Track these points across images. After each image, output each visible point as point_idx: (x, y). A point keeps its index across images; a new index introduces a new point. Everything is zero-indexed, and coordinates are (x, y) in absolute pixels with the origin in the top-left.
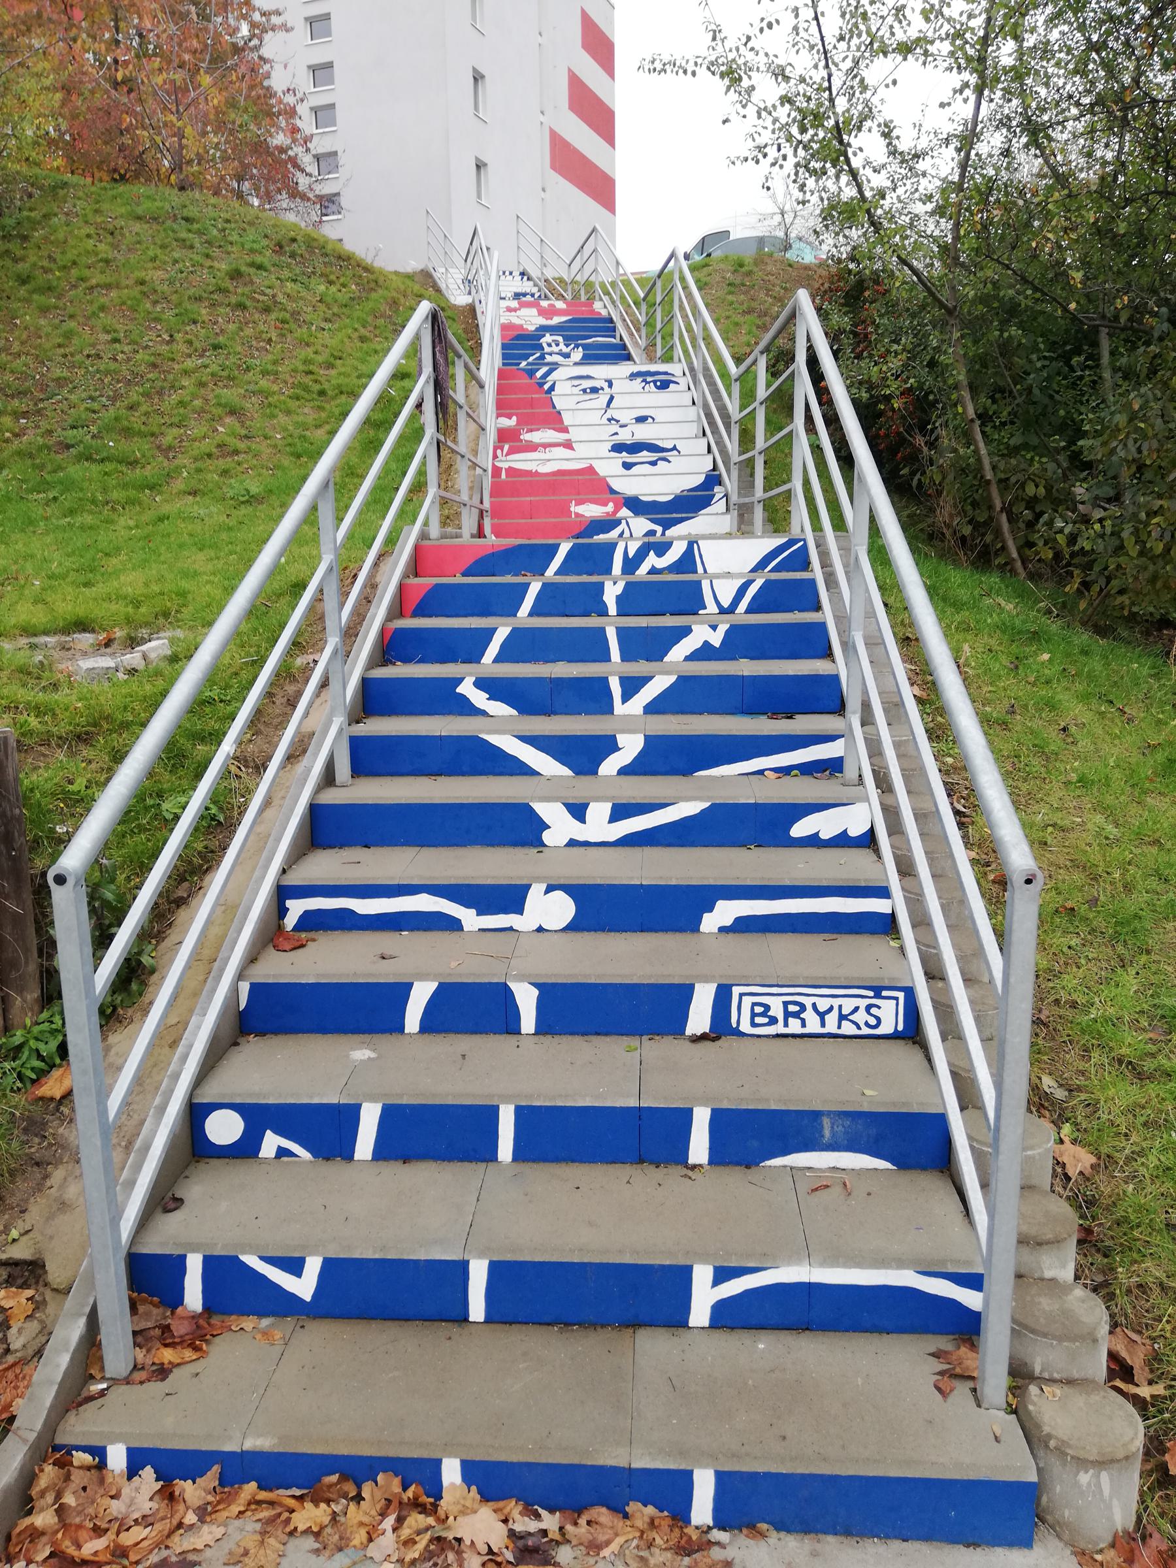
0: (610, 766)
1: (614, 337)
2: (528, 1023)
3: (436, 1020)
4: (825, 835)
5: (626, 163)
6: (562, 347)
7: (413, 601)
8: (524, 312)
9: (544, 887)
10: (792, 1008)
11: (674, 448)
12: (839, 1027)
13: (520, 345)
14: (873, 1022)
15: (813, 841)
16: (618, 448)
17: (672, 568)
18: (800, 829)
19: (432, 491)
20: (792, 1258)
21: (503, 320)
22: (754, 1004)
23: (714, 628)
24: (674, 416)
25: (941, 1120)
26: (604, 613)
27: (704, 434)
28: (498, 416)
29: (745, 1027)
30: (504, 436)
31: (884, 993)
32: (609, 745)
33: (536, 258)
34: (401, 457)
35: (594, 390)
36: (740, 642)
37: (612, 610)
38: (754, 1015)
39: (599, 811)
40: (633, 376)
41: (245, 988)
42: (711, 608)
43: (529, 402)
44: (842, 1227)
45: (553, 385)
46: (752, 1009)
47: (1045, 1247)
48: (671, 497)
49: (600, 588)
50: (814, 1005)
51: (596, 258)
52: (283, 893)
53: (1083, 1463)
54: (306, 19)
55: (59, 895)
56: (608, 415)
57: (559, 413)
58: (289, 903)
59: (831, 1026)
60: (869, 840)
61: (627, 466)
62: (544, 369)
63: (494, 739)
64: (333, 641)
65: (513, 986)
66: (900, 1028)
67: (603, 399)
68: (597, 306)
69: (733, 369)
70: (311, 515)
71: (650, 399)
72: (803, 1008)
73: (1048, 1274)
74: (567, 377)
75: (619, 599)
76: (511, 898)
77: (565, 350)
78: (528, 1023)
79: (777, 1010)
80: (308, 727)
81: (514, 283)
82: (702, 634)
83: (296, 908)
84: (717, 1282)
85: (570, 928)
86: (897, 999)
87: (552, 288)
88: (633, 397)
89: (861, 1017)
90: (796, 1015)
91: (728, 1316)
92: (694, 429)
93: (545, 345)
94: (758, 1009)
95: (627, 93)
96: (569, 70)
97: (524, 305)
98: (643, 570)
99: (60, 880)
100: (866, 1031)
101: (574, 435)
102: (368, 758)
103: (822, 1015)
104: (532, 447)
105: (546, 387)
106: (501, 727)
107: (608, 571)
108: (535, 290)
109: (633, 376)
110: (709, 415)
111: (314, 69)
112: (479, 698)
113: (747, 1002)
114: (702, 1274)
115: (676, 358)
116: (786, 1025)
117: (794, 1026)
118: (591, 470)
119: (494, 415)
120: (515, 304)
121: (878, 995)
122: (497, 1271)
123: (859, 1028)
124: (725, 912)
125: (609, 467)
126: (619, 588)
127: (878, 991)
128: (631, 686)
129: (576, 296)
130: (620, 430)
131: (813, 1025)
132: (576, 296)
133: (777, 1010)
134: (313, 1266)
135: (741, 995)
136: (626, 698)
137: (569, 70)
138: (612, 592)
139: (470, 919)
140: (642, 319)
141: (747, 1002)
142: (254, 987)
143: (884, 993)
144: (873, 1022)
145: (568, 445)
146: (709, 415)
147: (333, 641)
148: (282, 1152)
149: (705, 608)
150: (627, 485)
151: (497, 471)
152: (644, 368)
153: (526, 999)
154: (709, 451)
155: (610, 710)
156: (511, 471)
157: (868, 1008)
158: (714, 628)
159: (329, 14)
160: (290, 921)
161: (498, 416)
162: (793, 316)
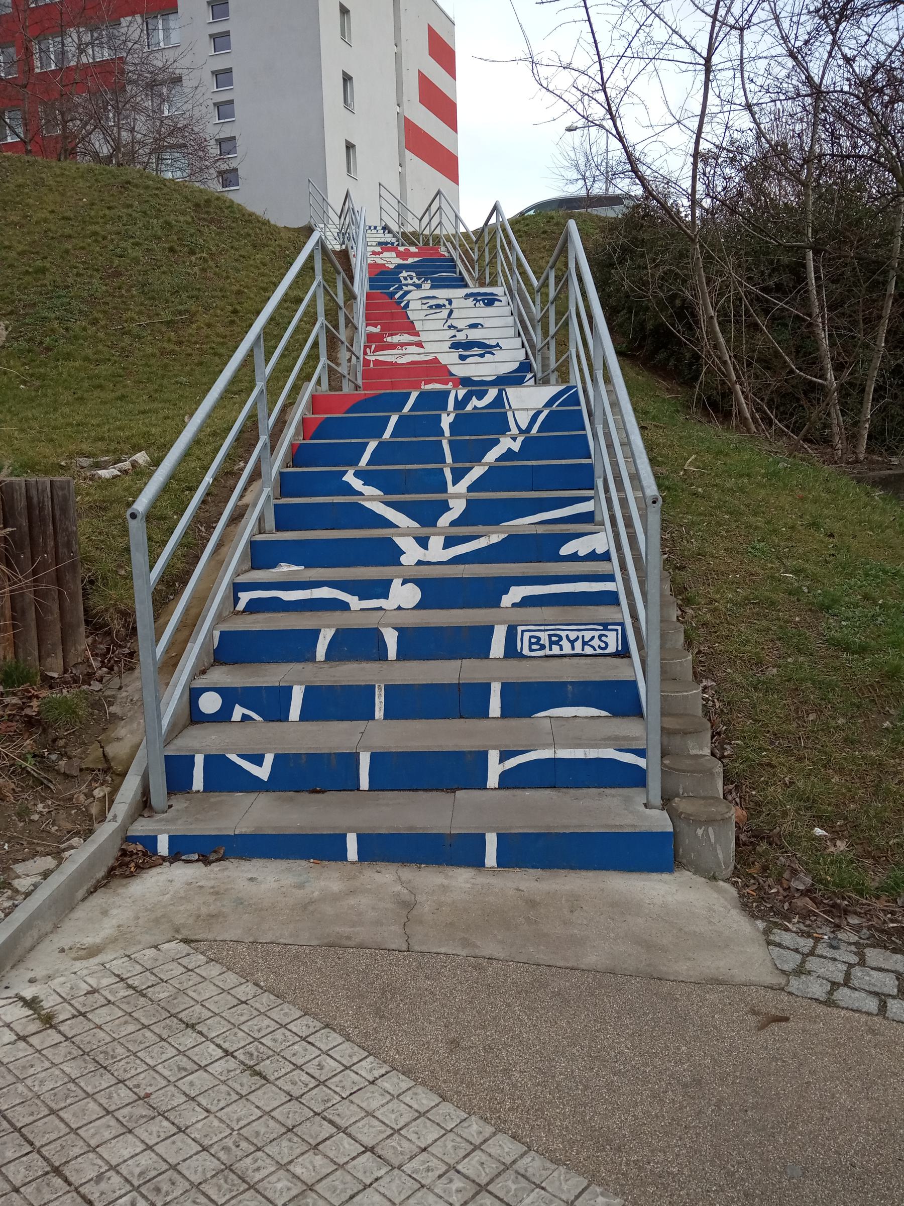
0: (444, 520)
1: (455, 273)
2: (392, 653)
3: (335, 652)
4: (581, 554)
5: (467, 144)
6: (415, 280)
7: (313, 429)
8: (386, 255)
9: (400, 581)
10: (554, 639)
11: (498, 345)
12: (583, 650)
13: (383, 278)
14: (603, 645)
15: (574, 557)
16: (456, 346)
17: (488, 406)
18: (565, 550)
19: (323, 360)
20: (544, 746)
21: (369, 261)
22: (531, 637)
23: (514, 439)
24: (497, 323)
25: (634, 683)
26: (442, 433)
27: (519, 335)
28: (367, 325)
29: (526, 651)
30: (370, 337)
31: (610, 627)
32: (444, 507)
33: (395, 215)
34: (302, 332)
35: (438, 306)
36: (531, 447)
37: (447, 433)
38: (531, 644)
39: (436, 542)
40: (467, 296)
41: (217, 634)
42: (514, 431)
43: (391, 316)
44: (573, 733)
45: (408, 302)
46: (530, 640)
47: (689, 735)
48: (494, 378)
49: (439, 418)
50: (567, 636)
51: (441, 214)
52: (237, 588)
53: (699, 823)
54: (210, 36)
55: (133, 524)
56: (449, 323)
57: (412, 322)
58: (240, 594)
59: (578, 649)
60: (606, 557)
61: (462, 358)
62: (401, 293)
63: (368, 504)
64: (263, 439)
65: (383, 630)
66: (620, 648)
67: (445, 313)
68: (442, 250)
69: (535, 283)
70: (250, 355)
71: (482, 312)
72: (561, 638)
73: (692, 752)
74: (417, 298)
75: (451, 425)
76: (381, 589)
77: (417, 282)
78: (392, 653)
79: (545, 640)
80: (245, 500)
81: (378, 235)
82: (506, 443)
83: (245, 597)
84: (501, 761)
85: (418, 607)
86: (617, 630)
87: (409, 238)
88: (466, 310)
89: (596, 643)
90: (557, 643)
91: (508, 780)
92: (511, 332)
93: (402, 279)
94: (533, 640)
95: (467, 89)
96: (419, 71)
97: (384, 250)
98: (469, 408)
99: (133, 516)
100: (599, 651)
101: (423, 337)
102: (285, 518)
103: (572, 643)
104: (393, 346)
105: (402, 305)
106: (373, 499)
107: (445, 408)
108: (394, 240)
109: (467, 296)
110: (522, 322)
111: (216, 74)
112: (357, 484)
113: (527, 635)
114: (493, 756)
115: (499, 283)
116: (551, 649)
117: (556, 650)
118: (436, 360)
119: (364, 324)
120: (378, 249)
121: (606, 629)
122: (374, 757)
123: (595, 650)
124: (516, 594)
125: (449, 359)
126: (451, 418)
127: (605, 626)
128: (458, 476)
129: (426, 243)
130: (457, 334)
131: (567, 649)
132: (426, 243)
133: (545, 640)
134: (269, 759)
135: (523, 631)
136: (454, 484)
137: (419, 71)
138: (446, 421)
139: (354, 602)
140: (475, 257)
141: (527, 635)
142: (222, 633)
143: (610, 627)
144: (603, 645)
145: (419, 344)
146: (522, 322)
147: (263, 439)
148: (245, 718)
149: (510, 430)
150: (460, 370)
151: (366, 362)
152: (475, 291)
153: (391, 638)
154: (523, 346)
155: (445, 490)
156: (376, 362)
157: (600, 637)
158: (514, 439)
159: (229, 32)
160: (241, 606)
161: (367, 325)
162: (566, 241)
